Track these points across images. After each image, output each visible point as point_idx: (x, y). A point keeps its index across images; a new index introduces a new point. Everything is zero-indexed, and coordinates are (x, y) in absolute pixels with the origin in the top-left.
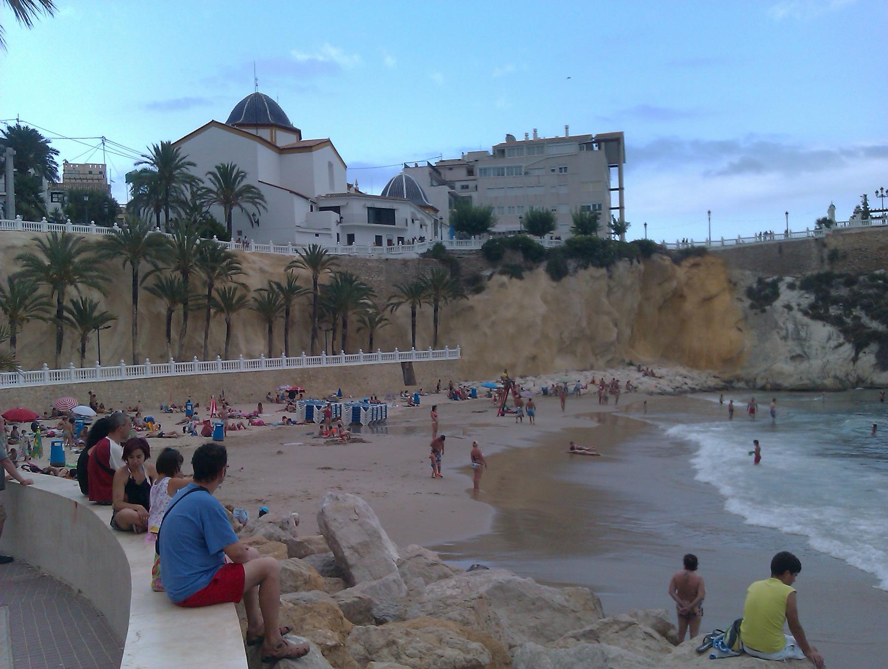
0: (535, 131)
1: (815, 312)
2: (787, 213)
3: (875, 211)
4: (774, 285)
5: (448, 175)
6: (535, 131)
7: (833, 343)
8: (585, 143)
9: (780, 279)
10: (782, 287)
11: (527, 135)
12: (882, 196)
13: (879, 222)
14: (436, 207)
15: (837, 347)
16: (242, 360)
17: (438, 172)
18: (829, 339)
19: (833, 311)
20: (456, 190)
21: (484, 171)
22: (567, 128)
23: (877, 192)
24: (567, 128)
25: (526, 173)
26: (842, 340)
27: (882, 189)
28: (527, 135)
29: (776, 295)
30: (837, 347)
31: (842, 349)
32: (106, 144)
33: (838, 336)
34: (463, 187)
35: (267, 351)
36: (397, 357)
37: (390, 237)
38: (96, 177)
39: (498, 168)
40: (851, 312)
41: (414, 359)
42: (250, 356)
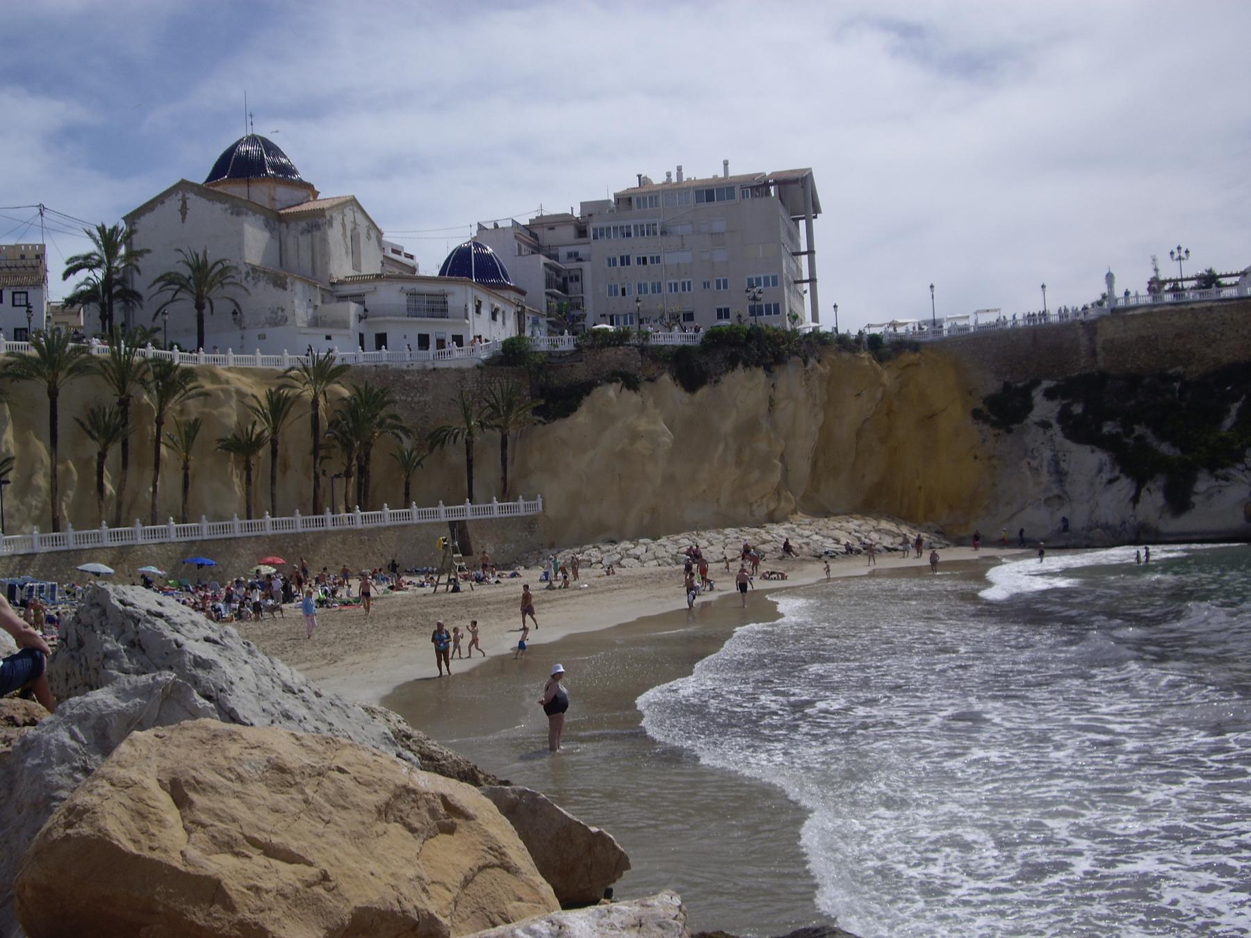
0: (679, 169)
1: (1078, 430)
2: (835, 306)
3: (1226, 276)
4: (1026, 393)
5: (547, 238)
6: (679, 169)
7: (1106, 476)
8: (757, 187)
9: (1036, 383)
10: (1037, 395)
11: (669, 175)
12: (1180, 258)
13: (1233, 292)
14: (521, 286)
15: (1111, 481)
16: (205, 524)
17: (535, 235)
18: (1100, 471)
19: (1108, 428)
20: (558, 257)
21: (600, 233)
22: (726, 164)
23: (1172, 253)
24: (726, 164)
25: (663, 233)
26: (1117, 473)
27: (1179, 248)
28: (669, 175)
29: (1029, 407)
30: (1111, 481)
31: (1117, 485)
32: (45, 214)
33: (1113, 469)
34: (570, 255)
35: (244, 510)
36: (443, 514)
37: (441, 336)
38: (29, 263)
39: (622, 228)
40: (1132, 431)
41: (469, 516)
42: (218, 517)
